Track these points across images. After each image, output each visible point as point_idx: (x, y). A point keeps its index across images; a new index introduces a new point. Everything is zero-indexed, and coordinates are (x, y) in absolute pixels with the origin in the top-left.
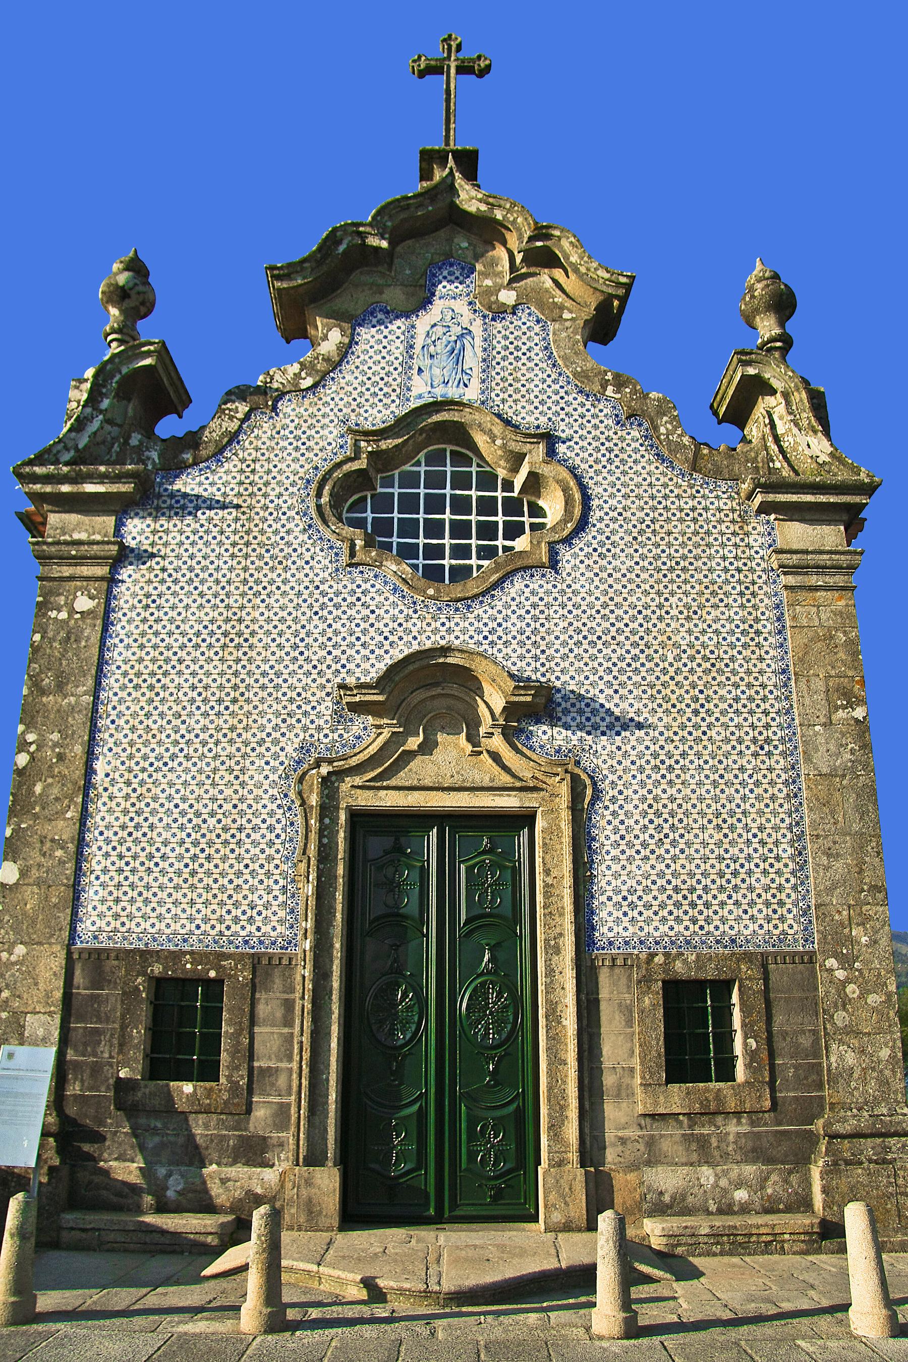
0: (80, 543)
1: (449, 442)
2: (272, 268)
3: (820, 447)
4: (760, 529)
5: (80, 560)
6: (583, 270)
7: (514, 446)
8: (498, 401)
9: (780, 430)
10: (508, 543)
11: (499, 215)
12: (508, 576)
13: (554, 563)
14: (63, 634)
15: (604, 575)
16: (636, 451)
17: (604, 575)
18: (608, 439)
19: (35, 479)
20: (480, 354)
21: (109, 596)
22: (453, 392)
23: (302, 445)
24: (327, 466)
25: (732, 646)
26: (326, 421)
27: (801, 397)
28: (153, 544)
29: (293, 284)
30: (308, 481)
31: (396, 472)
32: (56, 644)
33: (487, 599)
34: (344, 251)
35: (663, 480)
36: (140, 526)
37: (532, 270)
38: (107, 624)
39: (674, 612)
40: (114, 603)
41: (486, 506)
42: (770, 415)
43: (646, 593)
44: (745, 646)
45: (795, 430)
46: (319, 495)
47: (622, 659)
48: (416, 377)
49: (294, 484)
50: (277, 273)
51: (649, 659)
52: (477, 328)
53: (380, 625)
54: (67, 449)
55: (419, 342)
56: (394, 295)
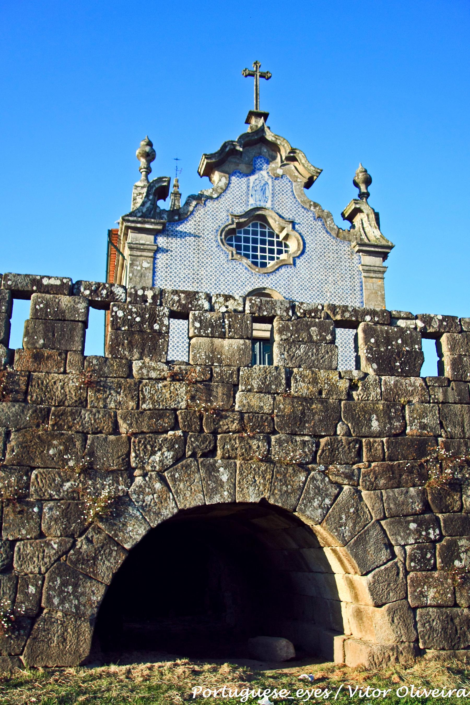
0: (142, 244)
1: (259, 220)
2: (205, 155)
3: (377, 233)
4: (357, 258)
5: (144, 250)
6: (306, 166)
7: (283, 225)
8: (277, 208)
9: (365, 226)
10: (278, 256)
11: (278, 142)
12: (280, 267)
13: (294, 264)
14: (139, 274)
15: (309, 269)
16: (320, 229)
17: (309, 269)
18: (311, 224)
19: (128, 221)
20: (271, 192)
21: (154, 263)
22: (262, 204)
23: (215, 218)
24: (223, 226)
25: (347, 293)
26: (222, 210)
27: (372, 216)
28: (167, 247)
29: (212, 161)
30: (217, 230)
31: (242, 229)
32: (137, 278)
33: (274, 274)
34: (229, 151)
35: (328, 239)
36: (162, 240)
37: (288, 162)
38: (154, 272)
39: (330, 282)
40: (156, 266)
41: (271, 243)
42: (362, 220)
43: (322, 275)
44: (351, 294)
45: (370, 227)
46: (221, 235)
47: (314, 295)
48: (250, 197)
49: (212, 231)
50: (208, 157)
51: (322, 296)
52: (270, 182)
53: (242, 279)
54: (139, 212)
55: (251, 185)
56: (243, 167)
